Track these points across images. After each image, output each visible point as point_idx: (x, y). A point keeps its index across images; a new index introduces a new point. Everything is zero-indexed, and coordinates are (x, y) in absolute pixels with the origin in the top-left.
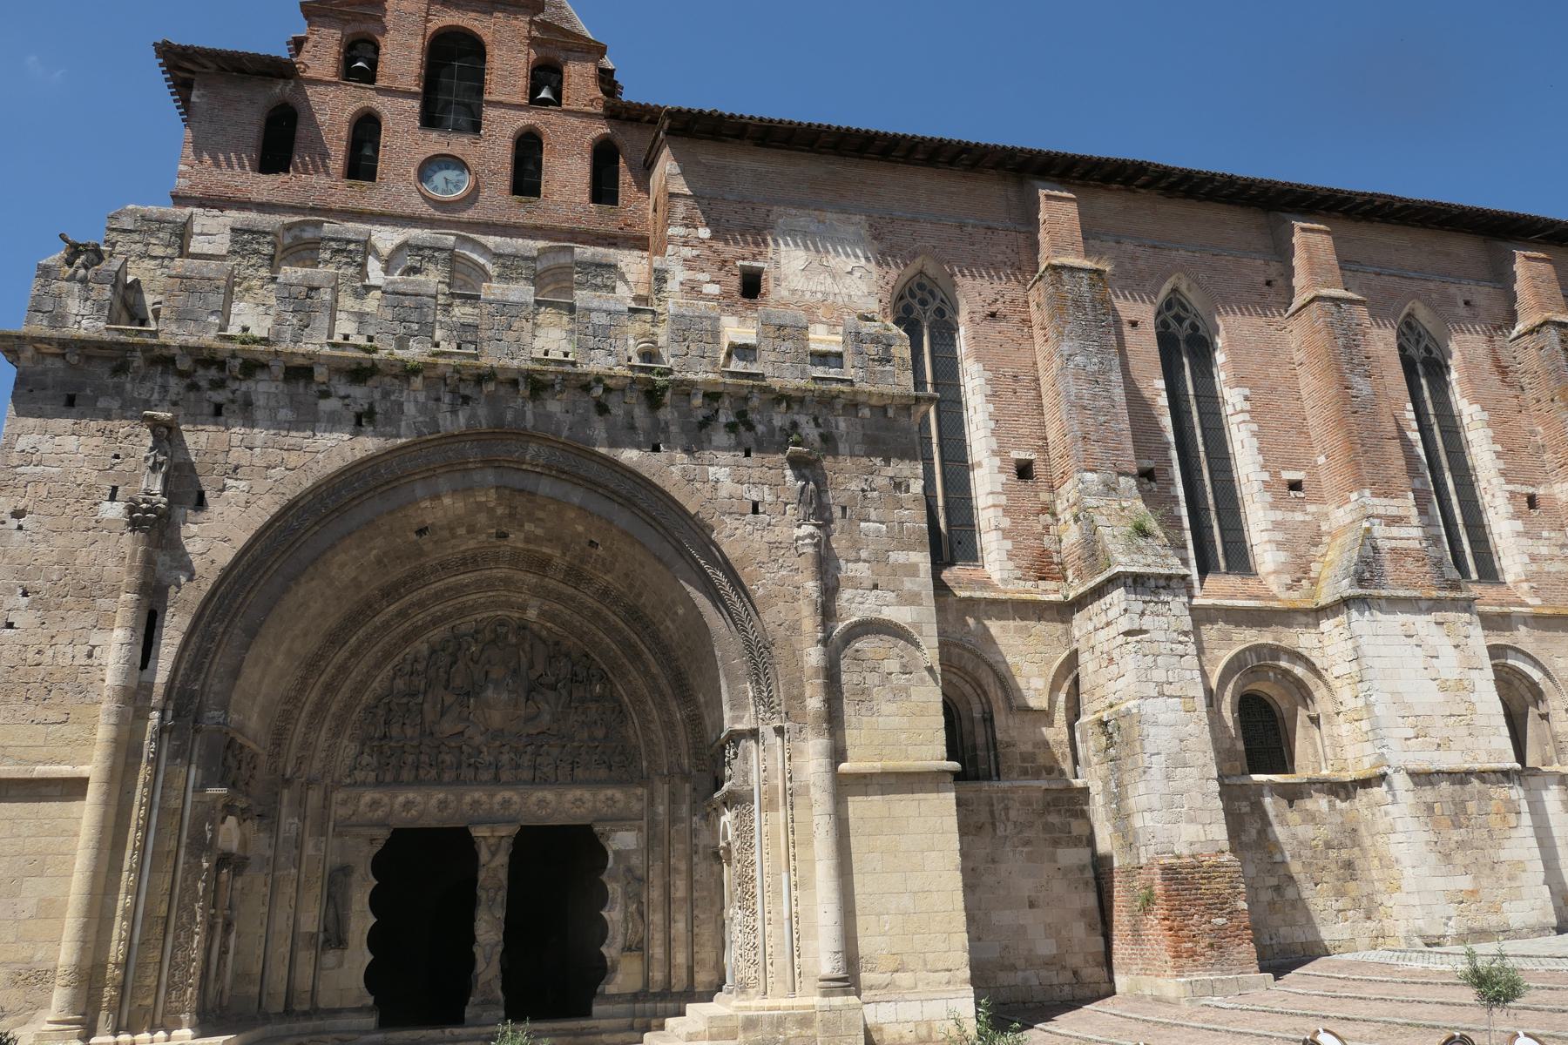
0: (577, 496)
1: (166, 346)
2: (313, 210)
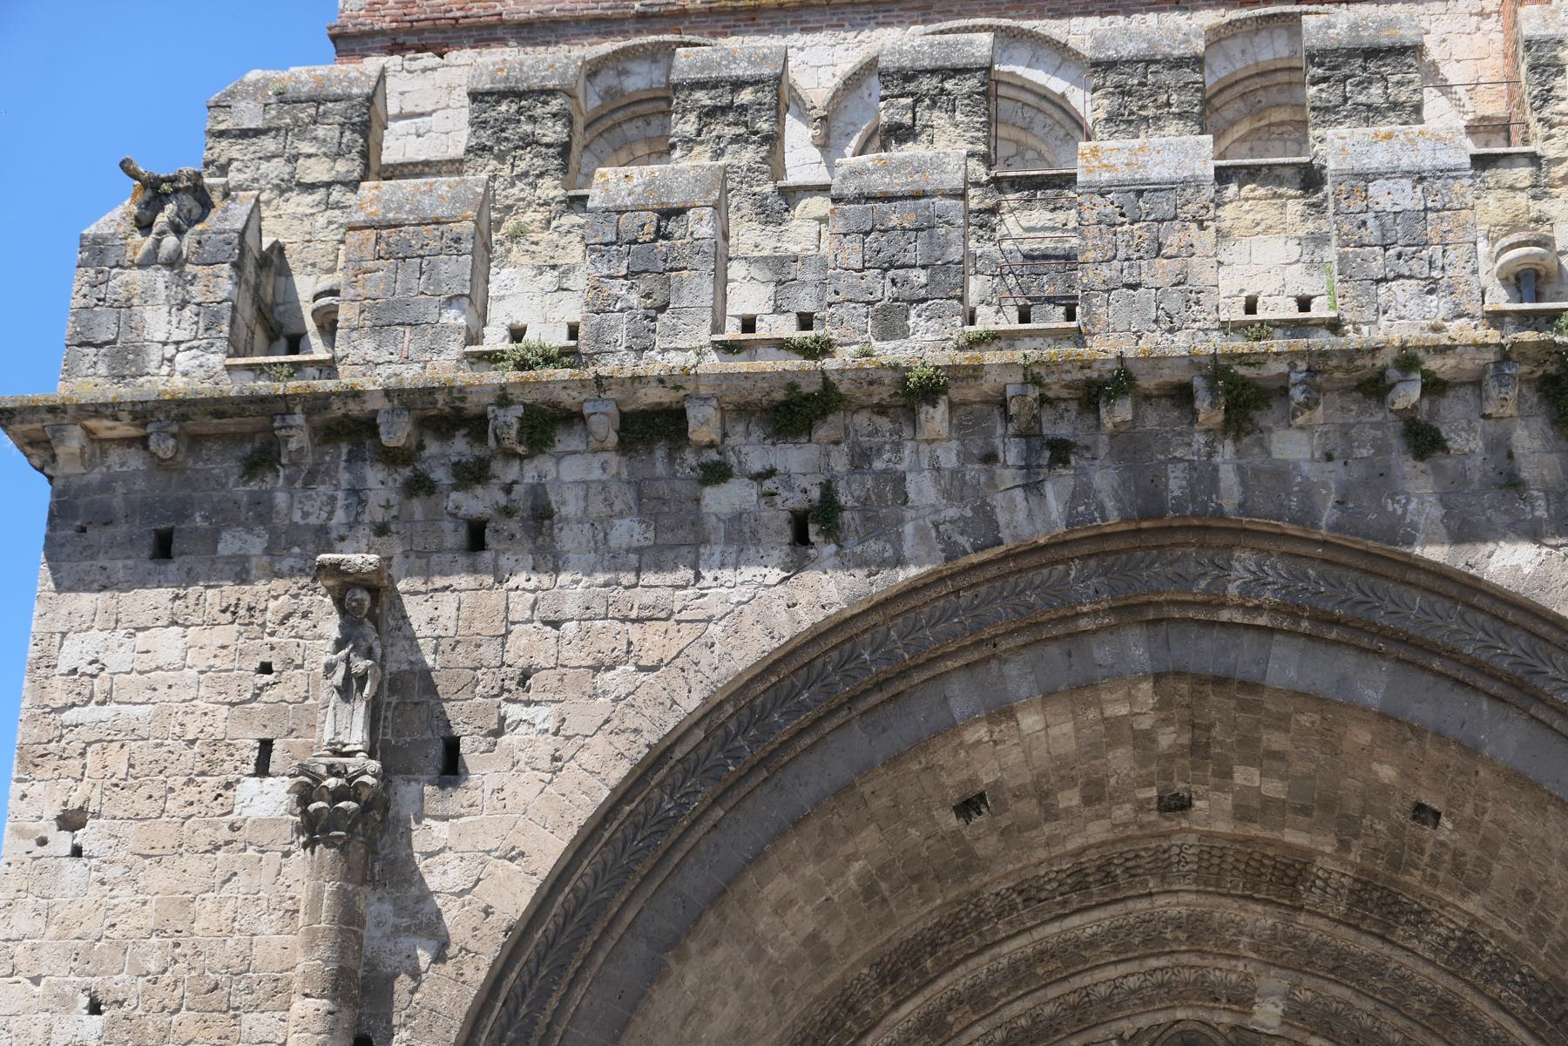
0: (1373, 684)
1: (356, 394)
2: (645, 20)
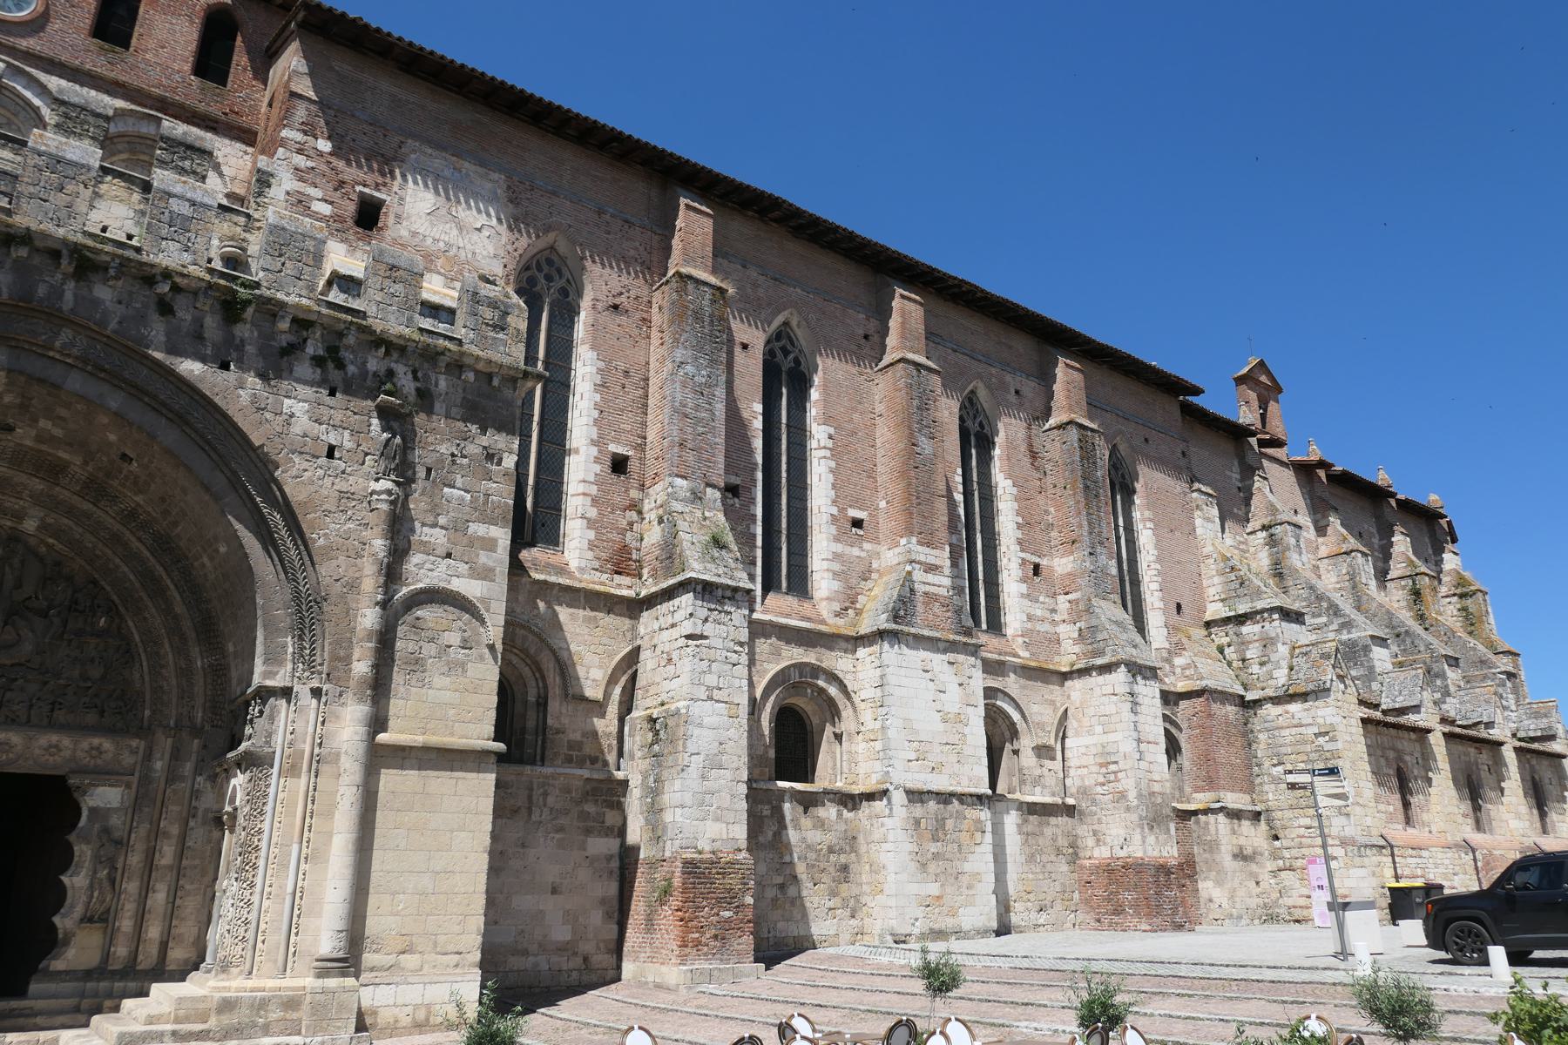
0: (115, 400)
